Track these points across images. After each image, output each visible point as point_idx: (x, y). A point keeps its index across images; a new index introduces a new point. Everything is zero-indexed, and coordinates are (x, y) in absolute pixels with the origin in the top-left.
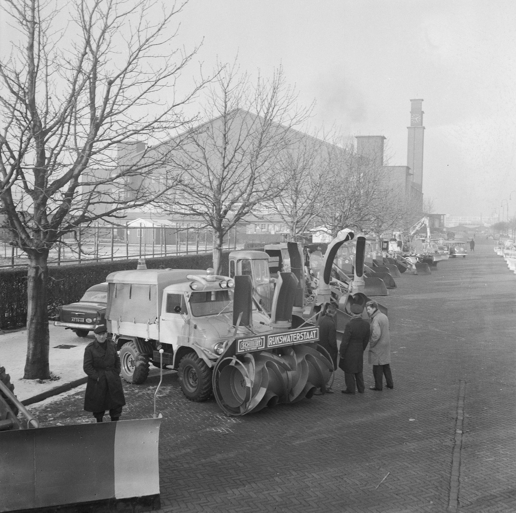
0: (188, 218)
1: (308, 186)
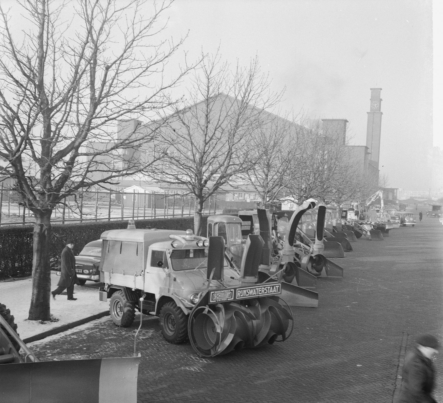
0: (173, 186)
1: (278, 161)
